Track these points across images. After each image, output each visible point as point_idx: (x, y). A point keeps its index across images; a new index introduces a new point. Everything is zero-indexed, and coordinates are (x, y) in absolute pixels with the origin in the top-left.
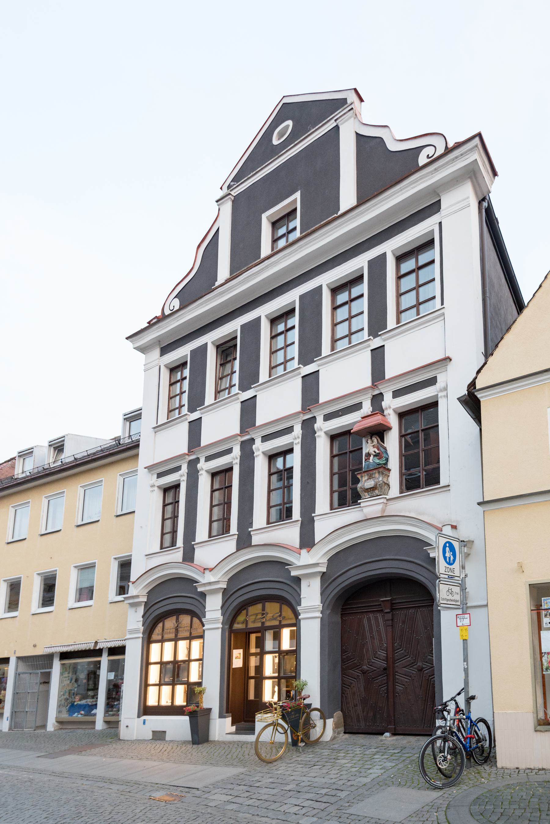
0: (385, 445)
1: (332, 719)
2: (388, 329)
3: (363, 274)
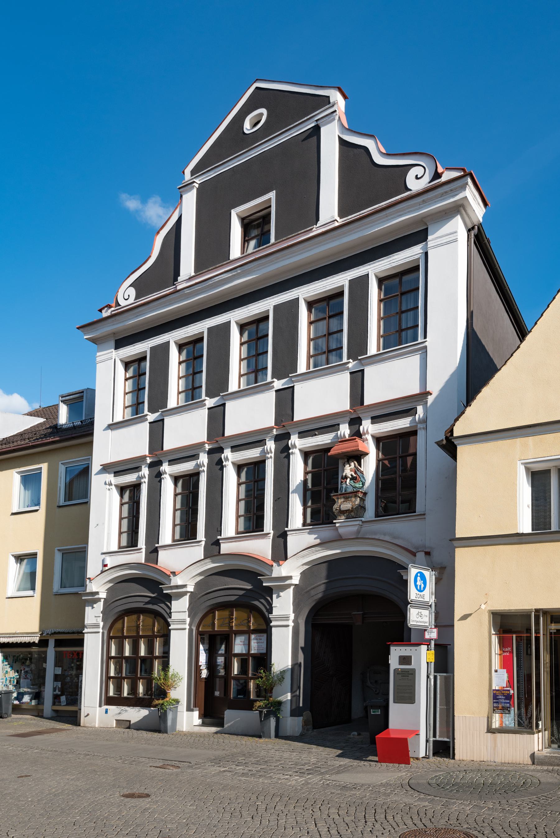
0: (362, 469)
1: (302, 718)
2: (369, 355)
3: (343, 291)
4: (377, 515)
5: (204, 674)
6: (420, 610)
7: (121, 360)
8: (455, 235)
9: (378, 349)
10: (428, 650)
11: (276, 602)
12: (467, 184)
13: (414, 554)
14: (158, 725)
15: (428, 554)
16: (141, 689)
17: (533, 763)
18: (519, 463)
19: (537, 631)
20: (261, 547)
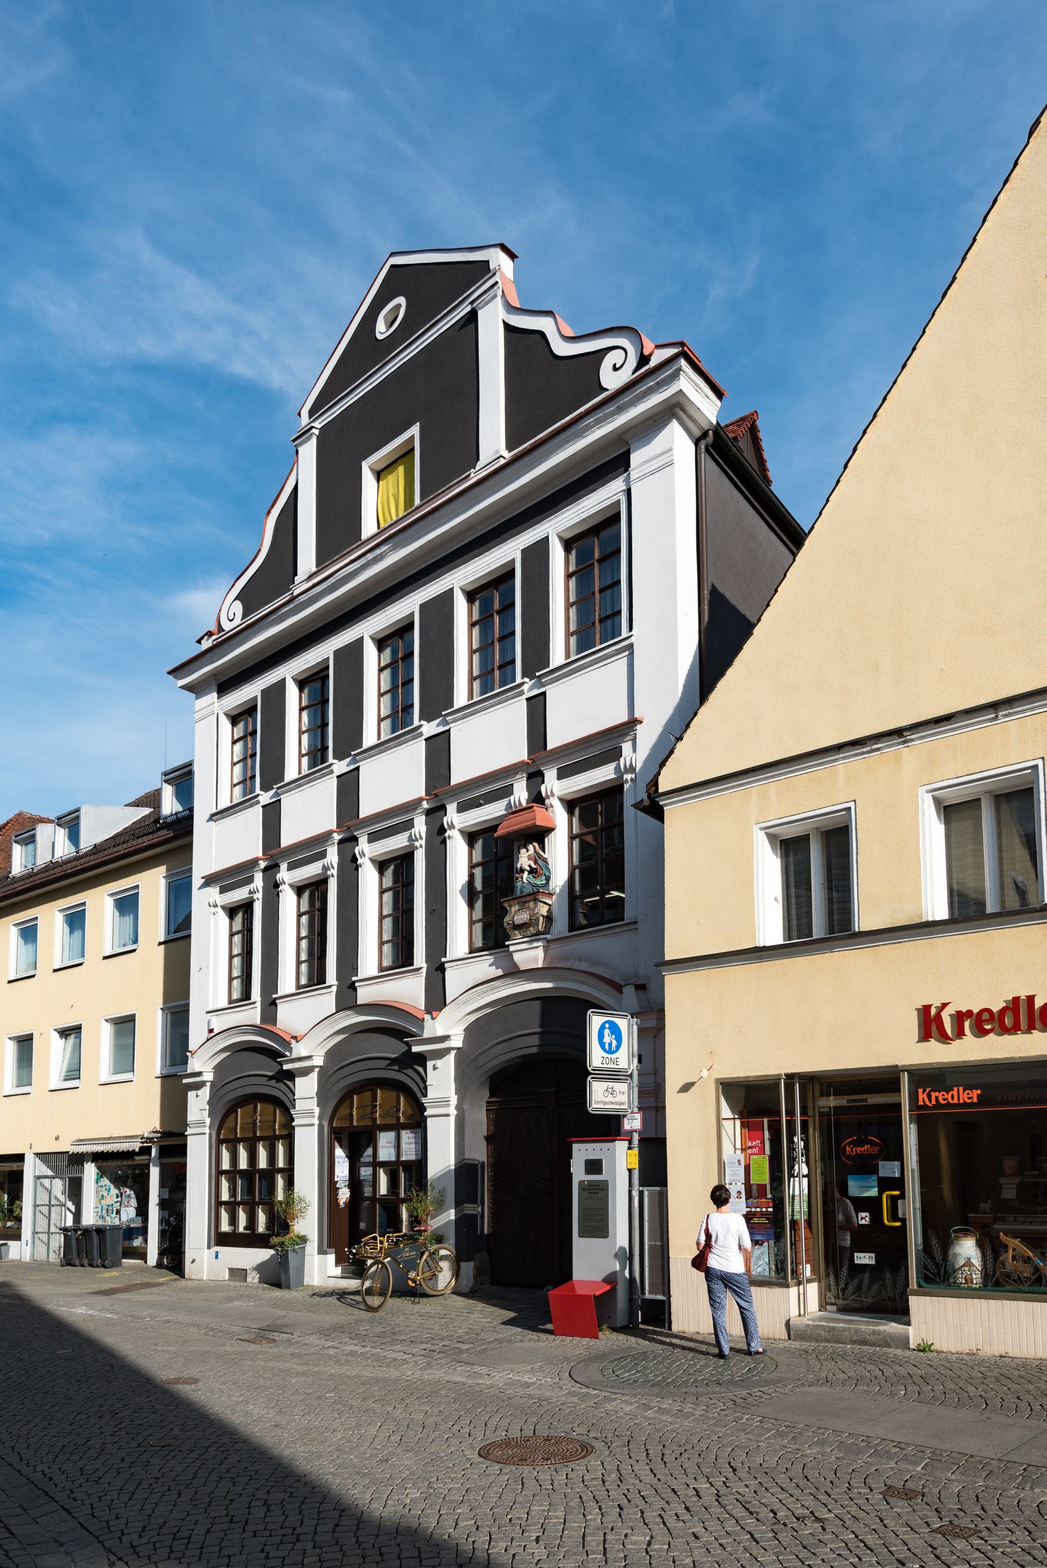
1: (473, 1263)
2: (552, 667)
4: (572, 928)
5: (344, 1195)
6: (611, 1084)
7: (226, 714)
8: (669, 454)
9: (568, 656)
10: (630, 1148)
11: (432, 1077)
12: (680, 369)
13: (619, 988)
14: (278, 1275)
15: (641, 988)
16: (262, 1218)
17: (789, 1338)
18: (756, 828)
19: (790, 1112)
20: (409, 990)
